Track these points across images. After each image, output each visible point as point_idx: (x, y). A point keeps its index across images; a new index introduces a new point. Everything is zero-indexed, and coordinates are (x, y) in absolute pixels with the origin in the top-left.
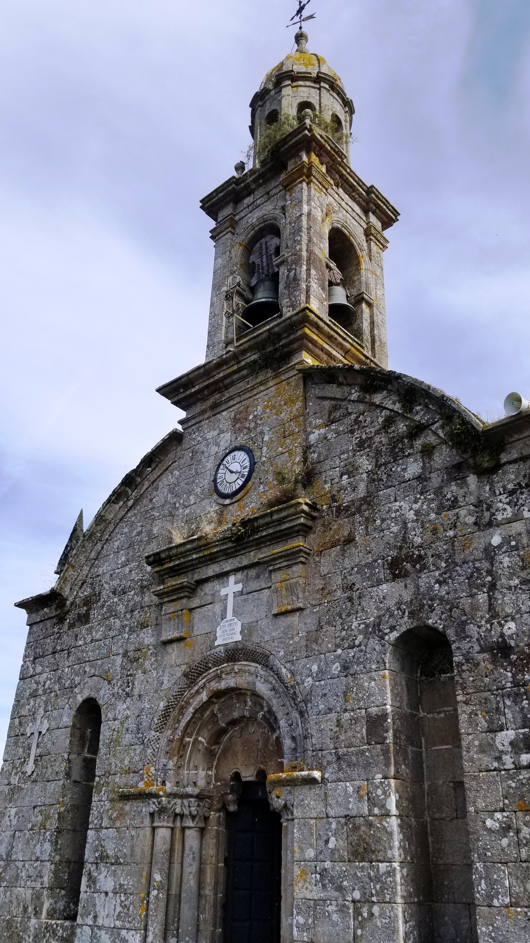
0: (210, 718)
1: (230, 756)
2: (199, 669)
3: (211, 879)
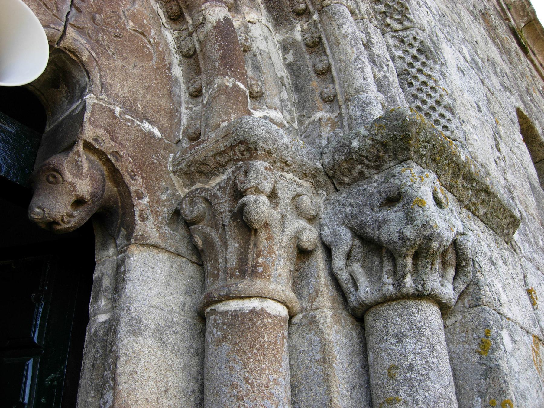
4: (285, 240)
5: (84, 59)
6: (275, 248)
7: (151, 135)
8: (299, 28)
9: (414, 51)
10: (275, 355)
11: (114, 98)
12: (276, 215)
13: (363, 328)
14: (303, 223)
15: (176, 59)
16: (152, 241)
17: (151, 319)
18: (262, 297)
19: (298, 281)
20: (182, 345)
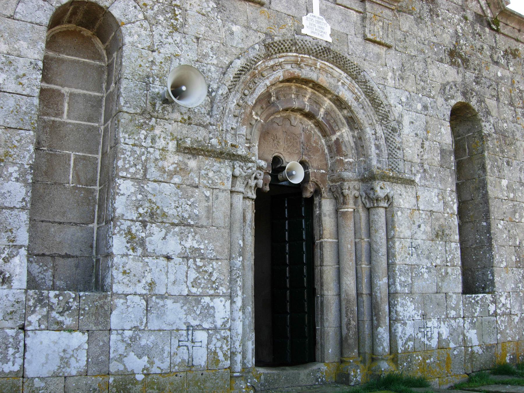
9: (390, 131)
12: (350, 192)
13: (369, 213)
14: (356, 192)
15: (325, 147)
17: (327, 213)
18: (348, 208)
19: (355, 203)
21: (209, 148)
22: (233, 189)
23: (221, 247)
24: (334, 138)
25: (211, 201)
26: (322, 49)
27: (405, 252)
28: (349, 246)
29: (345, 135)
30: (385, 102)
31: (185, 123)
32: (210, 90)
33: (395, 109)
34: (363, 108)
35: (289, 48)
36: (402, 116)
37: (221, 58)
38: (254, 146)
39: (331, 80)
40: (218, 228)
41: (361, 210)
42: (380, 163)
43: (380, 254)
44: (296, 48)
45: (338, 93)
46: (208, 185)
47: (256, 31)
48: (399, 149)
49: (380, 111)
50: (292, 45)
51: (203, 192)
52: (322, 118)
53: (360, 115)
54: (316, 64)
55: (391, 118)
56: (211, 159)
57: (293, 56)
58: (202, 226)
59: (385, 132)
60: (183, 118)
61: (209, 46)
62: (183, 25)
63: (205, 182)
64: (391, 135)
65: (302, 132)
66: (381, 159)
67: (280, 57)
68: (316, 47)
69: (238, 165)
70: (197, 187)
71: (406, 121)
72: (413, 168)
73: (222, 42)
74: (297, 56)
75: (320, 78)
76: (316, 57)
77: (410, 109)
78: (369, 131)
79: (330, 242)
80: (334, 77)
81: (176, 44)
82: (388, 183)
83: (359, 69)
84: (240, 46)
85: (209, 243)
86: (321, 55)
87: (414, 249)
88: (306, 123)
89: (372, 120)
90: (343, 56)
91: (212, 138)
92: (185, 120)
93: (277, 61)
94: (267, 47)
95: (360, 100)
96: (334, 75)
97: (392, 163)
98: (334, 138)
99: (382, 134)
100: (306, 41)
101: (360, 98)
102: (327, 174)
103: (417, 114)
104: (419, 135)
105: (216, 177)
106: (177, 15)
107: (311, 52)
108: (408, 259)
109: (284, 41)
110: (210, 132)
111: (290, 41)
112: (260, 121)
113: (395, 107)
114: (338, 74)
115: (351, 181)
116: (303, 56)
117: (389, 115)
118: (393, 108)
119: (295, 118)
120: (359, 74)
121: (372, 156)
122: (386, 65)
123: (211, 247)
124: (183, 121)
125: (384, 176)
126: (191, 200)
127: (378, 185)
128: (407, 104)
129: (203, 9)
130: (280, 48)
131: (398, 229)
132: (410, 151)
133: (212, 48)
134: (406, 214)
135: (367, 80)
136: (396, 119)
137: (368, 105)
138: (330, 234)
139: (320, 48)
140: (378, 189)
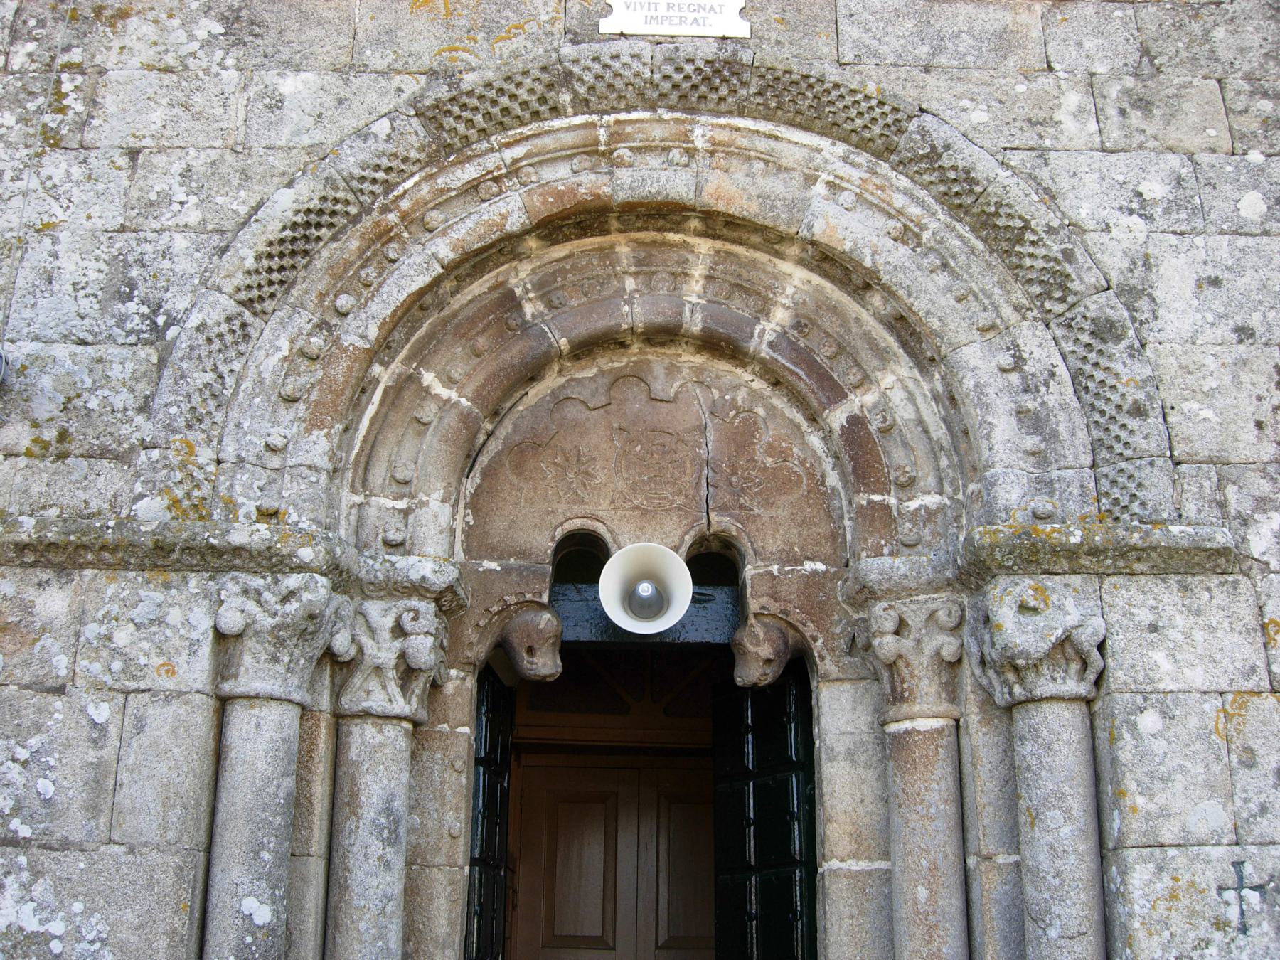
0: (487, 310)
1: (551, 472)
2: (504, 101)
3: (452, 923)
4: (925, 660)
5: (734, 533)
6: (916, 672)
7: (815, 573)
8: (937, 376)
9: (1086, 338)
10: (926, 767)
11: (768, 560)
14: (942, 638)
16: (833, 676)
19: (952, 691)
20: (875, 759)
21: (109, 536)
22: (227, 687)
23: (141, 926)
24: (837, 418)
25: (113, 740)
26: (698, 70)
27: (1193, 913)
28: (922, 893)
29: (897, 396)
30: (1043, 218)
31: (43, 458)
32: (161, 320)
33: (1104, 238)
34: (945, 266)
35: (543, 100)
36: (1147, 265)
37: (220, 200)
38: (422, 504)
39: (776, 186)
40: (131, 851)
41: (973, 718)
42: (1051, 493)
43: (1053, 933)
44: (575, 92)
45: (810, 228)
46: (107, 678)
47: (387, 73)
48: (1138, 411)
49: (1028, 262)
50: (550, 86)
51: (84, 710)
52: (771, 345)
53: (930, 297)
54: (686, 137)
55: (1083, 278)
56: (133, 574)
57: (570, 128)
58: (65, 845)
59: (1068, 347)
60: (36, 441)
61: (177, 167)
62: (83, 124)
63: (97, 667)
64: (1093, 356)
65: (706, 418)
66: (1055, 474)
67: (508, 145)
68: (669, 69)
69: (237, 589)
70: (60, 690)
71: (1174, 279)
72: (1231, 490)
73: (230, 142)
74: (592, 125)
75: (709, 188)
76: (684, 111)
77: (1199, 223)
78: (977, 362)
79: (852, 875)
80: (788, 169)
81: (46, 190)
82: (1076, 580)
83: (895, 110)
84: (306, 140)
85: (88, 913)
86: (703, 98)
87: (1253, 897)
88: (727, 379)
89: (996, 308)
90: (806, 77)
91: (141, 497)
92: (46, 446)
93: (491, 161)
94: (431, 116)
95: (926, 235)
96: (784, 162)
97: (1114, 482)
98: (837, 418)
99: (1057, 359)
100: (615, 57)
101: (923, 228)
102: (835, 577)
103: (1242, 242)
104: (1259, 329)
105: (145, 645)
106: (66, 95)
107: (655, 95)
108: (1213, 950)
109: (508, 79)
110: (137, 475)
111: (537, 73)
112: (457, 404)
113: (1107, 229)
114: (802, 154)
115: (911, 592)
116: (623, 116)
117: (1068, 268)
118: (1089, 238)
119: (672, 370)
120: (900, 131)
121: (998, 469)
122: (1050, 68)
123: (95, 926)
124: (36, 450)
125: (1034, 549)
126: (31, 742)
127: (1004, 599)
128: (1172, 206)
129: (167, 51)
130: (495, 110)
131: (1140, 801)
132: (1208, 413)
133: (186, 174)
134: (1193, 722)
135: (939, 144)
136: (1114, 277)
137: (972, 250)
138: (857, 837)
139: (689, 68)
140: (1006, 615)
